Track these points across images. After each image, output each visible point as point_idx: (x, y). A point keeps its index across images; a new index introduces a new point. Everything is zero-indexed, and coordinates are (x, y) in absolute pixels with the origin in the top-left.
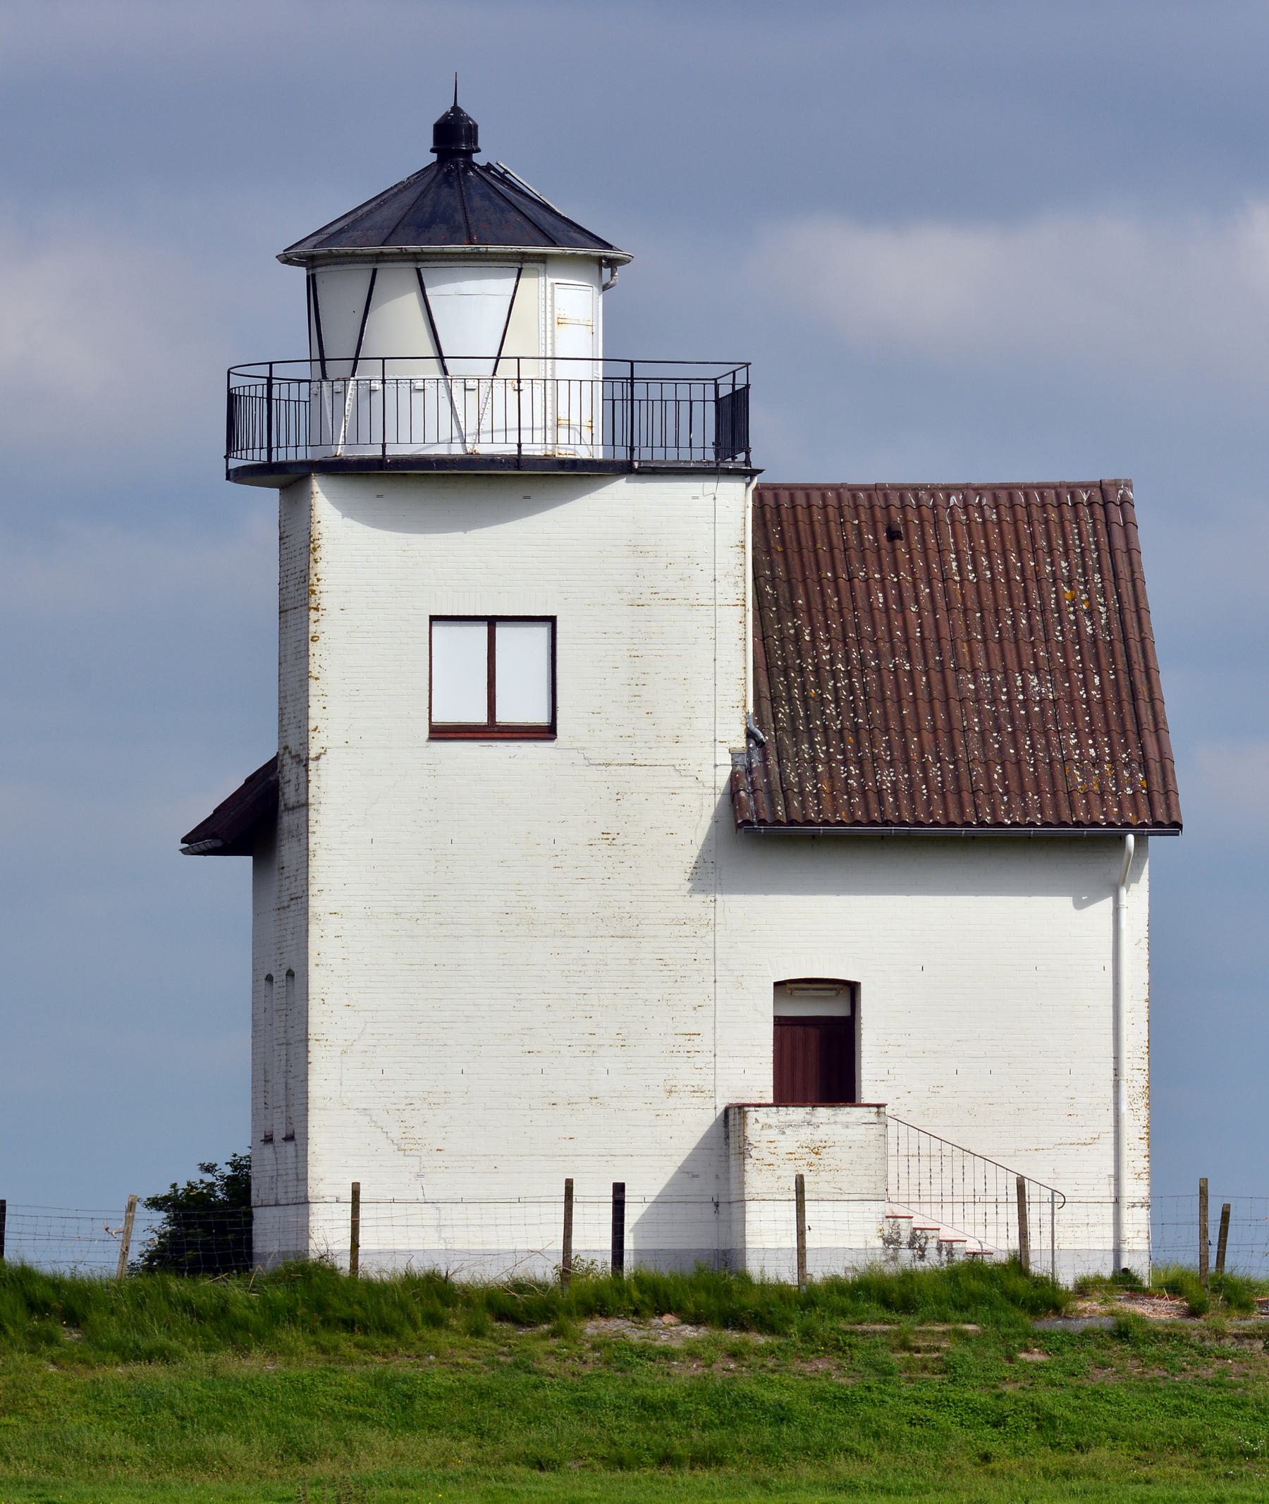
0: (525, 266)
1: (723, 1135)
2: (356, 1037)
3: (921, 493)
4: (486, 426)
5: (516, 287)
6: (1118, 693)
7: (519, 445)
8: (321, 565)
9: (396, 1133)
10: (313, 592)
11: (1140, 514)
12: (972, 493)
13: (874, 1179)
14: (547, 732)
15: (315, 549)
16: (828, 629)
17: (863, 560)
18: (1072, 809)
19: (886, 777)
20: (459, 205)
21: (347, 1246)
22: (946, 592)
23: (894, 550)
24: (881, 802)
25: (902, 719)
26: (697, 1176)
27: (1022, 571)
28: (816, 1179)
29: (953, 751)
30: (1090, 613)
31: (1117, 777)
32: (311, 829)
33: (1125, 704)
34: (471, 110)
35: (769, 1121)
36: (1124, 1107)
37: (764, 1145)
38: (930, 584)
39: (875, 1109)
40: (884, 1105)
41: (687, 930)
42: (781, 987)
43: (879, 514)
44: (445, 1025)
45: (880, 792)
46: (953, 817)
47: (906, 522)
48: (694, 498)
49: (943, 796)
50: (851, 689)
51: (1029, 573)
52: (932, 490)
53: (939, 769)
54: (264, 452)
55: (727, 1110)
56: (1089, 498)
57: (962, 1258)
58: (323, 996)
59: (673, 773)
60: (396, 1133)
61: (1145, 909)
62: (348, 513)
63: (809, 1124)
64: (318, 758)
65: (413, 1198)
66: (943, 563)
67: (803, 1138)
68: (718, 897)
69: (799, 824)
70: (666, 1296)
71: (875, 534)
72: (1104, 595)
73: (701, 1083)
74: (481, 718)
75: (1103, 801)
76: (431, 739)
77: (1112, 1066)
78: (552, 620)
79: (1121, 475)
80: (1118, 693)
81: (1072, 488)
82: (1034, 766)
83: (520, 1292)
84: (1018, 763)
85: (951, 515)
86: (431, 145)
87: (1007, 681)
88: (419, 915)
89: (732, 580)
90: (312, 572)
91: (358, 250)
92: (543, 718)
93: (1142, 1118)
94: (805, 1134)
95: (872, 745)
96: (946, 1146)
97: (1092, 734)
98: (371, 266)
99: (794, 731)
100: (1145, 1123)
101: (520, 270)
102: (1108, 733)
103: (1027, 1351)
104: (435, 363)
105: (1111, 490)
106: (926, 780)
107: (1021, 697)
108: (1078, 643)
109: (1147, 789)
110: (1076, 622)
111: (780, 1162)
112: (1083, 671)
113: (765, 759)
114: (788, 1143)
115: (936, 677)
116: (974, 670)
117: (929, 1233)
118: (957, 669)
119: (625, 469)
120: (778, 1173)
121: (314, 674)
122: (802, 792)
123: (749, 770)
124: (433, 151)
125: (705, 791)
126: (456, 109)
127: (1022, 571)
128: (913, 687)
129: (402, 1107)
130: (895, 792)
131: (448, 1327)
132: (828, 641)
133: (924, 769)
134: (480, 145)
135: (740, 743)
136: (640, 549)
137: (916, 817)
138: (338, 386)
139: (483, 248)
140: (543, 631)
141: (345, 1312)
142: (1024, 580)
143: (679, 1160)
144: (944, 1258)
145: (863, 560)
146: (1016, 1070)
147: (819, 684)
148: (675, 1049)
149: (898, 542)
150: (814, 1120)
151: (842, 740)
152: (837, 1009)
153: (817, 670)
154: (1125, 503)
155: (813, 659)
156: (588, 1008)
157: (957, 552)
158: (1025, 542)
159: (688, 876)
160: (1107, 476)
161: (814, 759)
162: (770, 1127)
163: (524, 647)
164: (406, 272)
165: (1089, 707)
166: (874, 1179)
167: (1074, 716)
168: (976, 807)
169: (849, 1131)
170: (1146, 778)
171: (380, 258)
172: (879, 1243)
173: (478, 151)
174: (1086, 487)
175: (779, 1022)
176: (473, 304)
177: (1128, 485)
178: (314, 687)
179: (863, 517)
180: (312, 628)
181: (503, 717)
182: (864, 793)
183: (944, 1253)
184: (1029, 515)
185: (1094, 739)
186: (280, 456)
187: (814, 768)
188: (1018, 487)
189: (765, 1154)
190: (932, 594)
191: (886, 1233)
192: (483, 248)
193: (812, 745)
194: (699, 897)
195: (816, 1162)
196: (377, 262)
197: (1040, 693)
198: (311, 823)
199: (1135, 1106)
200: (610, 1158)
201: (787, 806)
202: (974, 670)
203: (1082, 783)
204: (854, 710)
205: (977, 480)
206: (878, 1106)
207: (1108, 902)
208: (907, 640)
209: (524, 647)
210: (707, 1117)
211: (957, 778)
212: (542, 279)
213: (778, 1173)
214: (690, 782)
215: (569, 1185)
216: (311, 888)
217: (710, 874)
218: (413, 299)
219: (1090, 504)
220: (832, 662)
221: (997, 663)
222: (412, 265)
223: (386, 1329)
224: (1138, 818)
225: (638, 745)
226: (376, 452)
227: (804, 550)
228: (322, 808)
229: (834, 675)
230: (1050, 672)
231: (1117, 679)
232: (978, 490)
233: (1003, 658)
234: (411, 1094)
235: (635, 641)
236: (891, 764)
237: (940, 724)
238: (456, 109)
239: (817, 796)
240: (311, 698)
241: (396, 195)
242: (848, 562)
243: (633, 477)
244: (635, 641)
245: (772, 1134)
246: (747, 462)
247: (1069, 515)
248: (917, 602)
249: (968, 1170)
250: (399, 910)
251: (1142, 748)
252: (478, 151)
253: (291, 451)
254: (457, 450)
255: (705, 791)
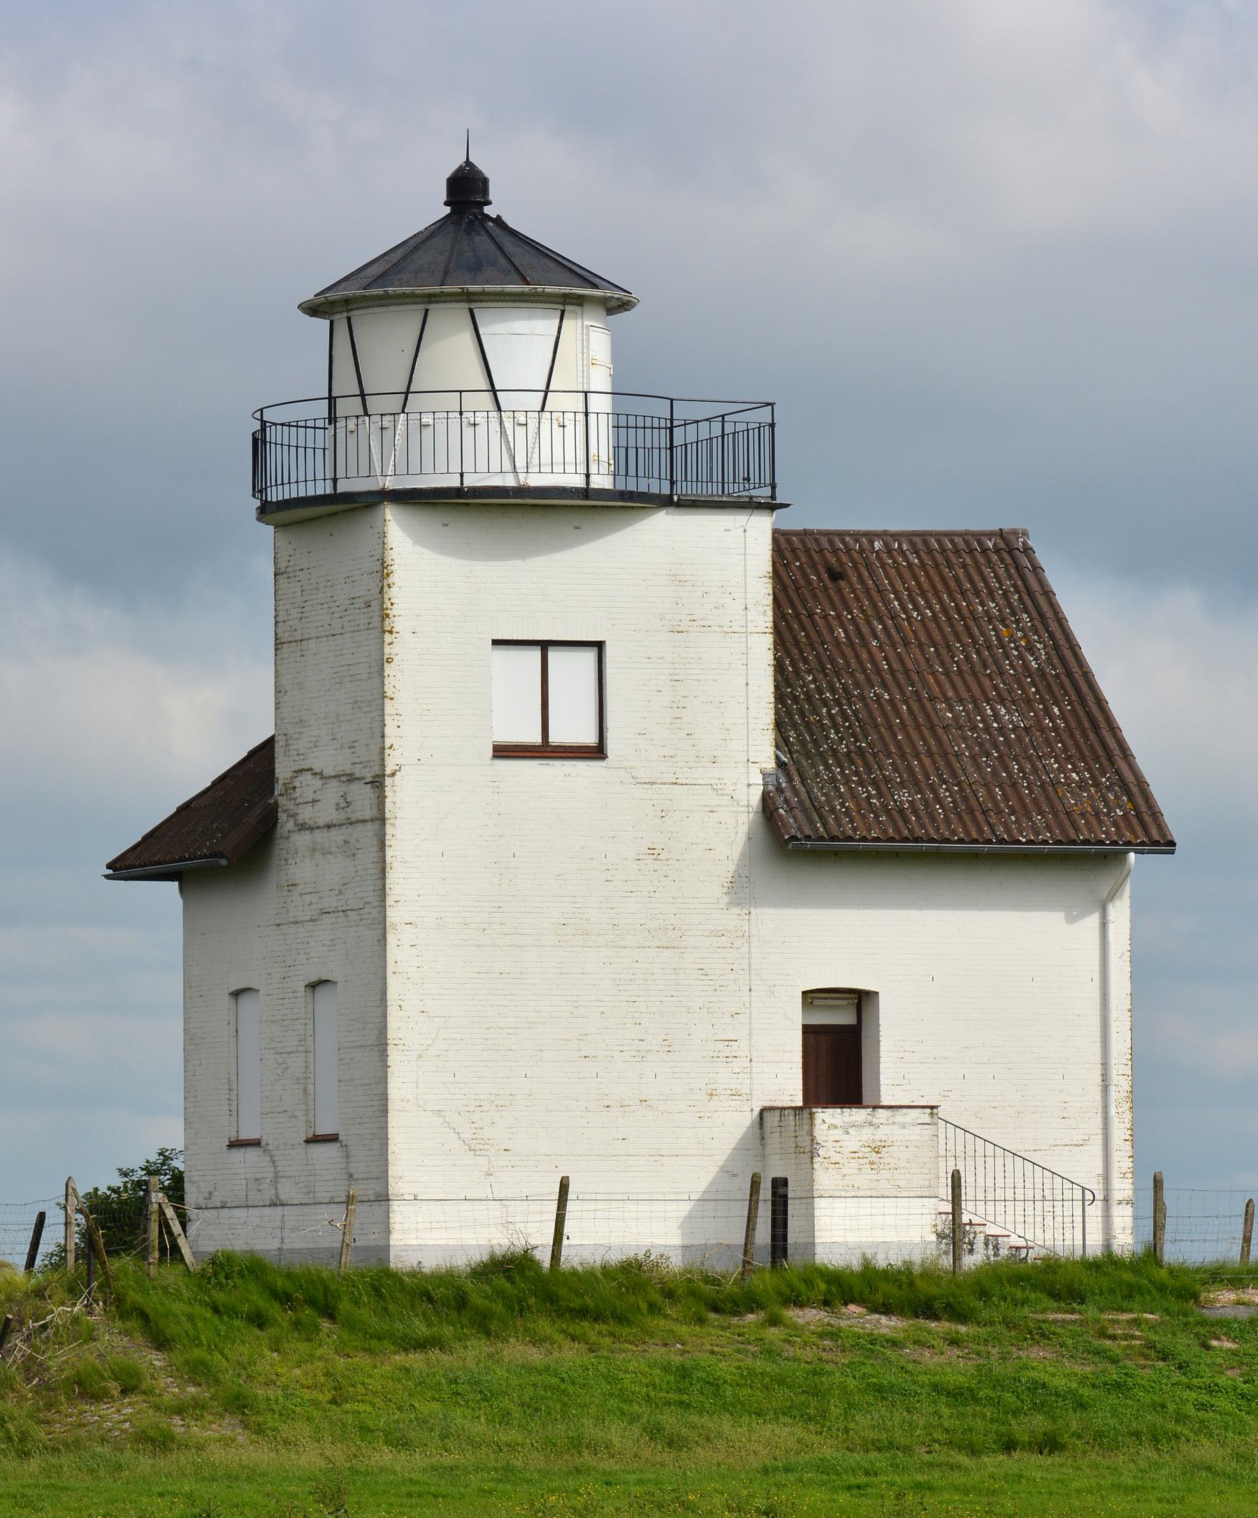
0: (568, 308)
1: (759, 1137)
2: (430, 1042)
3: (847, 539)
4: (535, 461)
5: (560, 328)
6: (1079, 723)
7: (588, 476)
8: (394, 590)
9: (467, 1135)
10: (388, 616)
11: (1042, 557)
12: (890, 539)
13: (928, 1177)
14: (597, 752)
15: (388, 575)
16: (805, 661)
17: (815, 598)
18: (1077, 829)
19: (904, 796)
20: (471, 252)
21: (550, 1240)
22: (898, 628)
23: (839, 590)
24: (906, 821)
25: (898, 743)
26: (735, 1175)
27: (959, 611)
28: (877, 1177)
29: (953, 773)
30: (1031, 649)
31: (1105, 800)
32: (387, 843)
33: (1089, 732)
34: (481, 163)
35: (834, 1122)
36: (1113, 1111)
37: (830, 1144)
38: (881, 621)
39: (928, 1111)
40: (936, 1107)
41: (724, 941)
42: (811, 998)
43: (816, 557)
44: (511, 1031)
45: (901, 811)
46: (975, 835)
47: (842, 564)
48: (727, 530)
49: (959, 815)
50: (843, 713)
51: (965, 612)
52: (856, 536)
53: (946, 790)
54: (329, 483)
55: (762, 1111)
56: (994, 545)
57: (1006, 1252)
58: (400, 1003)
59: (711, 791)
60: (467, 1135)
61: (1127, 924)
62: (418, 541)
63: (870, 1124)
64: (393, 775)
65: (484, 1197)
66: (887, 603)
67: (865, 1138)
68: (752, 910)
69: (839, 840)
70: (851, 1288)
71: (818, 575)
72: (1036, 632)
73: (739, 1087)
74: (537, 739)
75: (1100, 822)
76: (495, 757)
77: (1099, 1072)
78: (599, 646)
79: (1019, 526)
80: (1079, 723)
81: (979, 536)
82: (1028, 788)
83: (706, 1283)
84: (1014, 785)
85: (879, 558)
86: (445, 199)
87: (980, 711)
88: (485, 926)
89: (761, 608)
90: (386, 597)
91: (418, 290)
92: (590, 739)
93: (1126, 1121)
94: (867, 1134)
95: (881, 768)
96: (989, 1146)
97: (1069, 759)
98: (422, 307)
99: (808, 755)
100: (1129, 1126)
101: (563, 312)
102: (1083, 759)
103: (1218, 1339)
104: (488, 396)
105: (1012, 538)
106: (938, 800)
107: (995, 725)
108: (1029, 676)
109: (1135, 810)
110: (1020, 657)
111: (845, 1161)
112: (1042, 701)
113: (790, 780)
114: (852, 1142)
115: (915, 706)
116: (947, 700)
117: (978, 1229)
118: (932, 699)
119: (666, 502)
120: (844, 1171)
121: (389, 694)
122: (833, 810)
123: (779, 790)
124: (446, 204)
125: (740, 809)
126: (468, 162)
127: (959, 611)
128: (898, 714)
129: (473, 1108)
130: (915, 812)
131: (666, 1317)
132: (809, 672)
133: (933, 789)
134: (491, 198)
135: (771, 765)
136: (679, 578)
137: (942, 834)
138: (387, 421)
139: (540, 288)
140: (590, 656)
141: (576, 1303)
142: (963, 619)
143: (721, 1159)
144: (991, 1252)
145: (815, 598)
146: (1016, 1075)
147: (815, 712)
148: (715, 1055)
149: (842, 583)
150: (875, 1121)
151: (852, 762)
152: (844, 1018)
153: (809, 697)
154: (1027, 550)
155: (802, 687)
156: (637, 1015)
157: (895, 592)
158: (953, 584)
159: (725, 890)
160: (1007, 526)
161: (833, 780)
162: (836, 1127)
163: (572, 672)
164: (459, 312)
165: (1058, 735)
166: (928, 1177)
167: (1047, 741)
168: (991, 826)
169: (904, 1131)
170: (1130, 800)
171: (431, 298)
172: (933, 1238)
173: (489, 203)
174: (989, 535)
175: (807, 1030)
176: (521, 340)
177: (1025, 534)
178: (389, 707)
179: (804, 560)
180: (387, 650)
181: (555, 738)
182: (888, 813)
183: (991, 1247)
184: (948, 560)
185: (1072, 764)
186: (343, 487)
187: (837, 789)
188: (930, 534)
189: (831, 1154)
190: (885, 629)
191: (939, 1228)
192: (540, 288)
193: (827, 767)
194: (736, 910)
195: (877, 1160)
196: (430, 302)
197: (1012, 722)
198: (388, 837)
199: (1121, 1110)
200: (658, 1158)
201: (825, 825)
202: (947, 700)
203: (1076, 804)
204: (854, 735)
205: (894, 527)
206: (932, 1107)
207: (1094, 919)
208: (878, 671)
209: (572, 672)
210: (746, 1119)
211: (965, 799)
212: (579, 321)
213: (844, 1171)
214: (726, 800)
215: (564, 1187)
216: (388, 899)
217: (742, 890)
218: (467, 337)
219: (997, 551)
220: (819, 690)
221: (964, 694)
222: (466, 305)
223: (621, 1319)
224: (1137, 838)
225: (680, 764)
226: (454, 482)
227: (816, 584)
228: (398, 823)
229: (825, 702)
230: (1014, 702)
231: (1073, 709)
232: (896, 536)
233: (969, 690)
234: (480, 1097)
235: (676, 666)
236: (902, 785)
237: (934, 749)
238: (468, 162)
239: (847, 814)
240: (386, 718)
241: (424, 241)
242: (804, 602)
243: (671, 509)
244: (676, 666)
245: (837, 1134)
246: (773, 497)
247: (981, 560)
248: (876, 637)
249: (1009, 1167)
250: (468, 920)
251: (1118, 772)
252: (489, 203)
253: (310, 484)
254: (510, 482)
255: (740, 809)
